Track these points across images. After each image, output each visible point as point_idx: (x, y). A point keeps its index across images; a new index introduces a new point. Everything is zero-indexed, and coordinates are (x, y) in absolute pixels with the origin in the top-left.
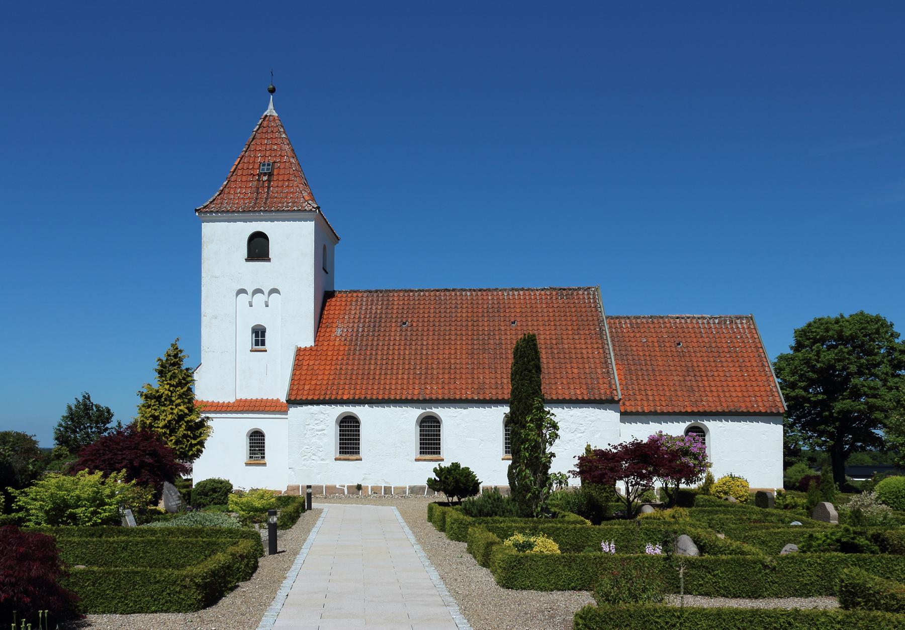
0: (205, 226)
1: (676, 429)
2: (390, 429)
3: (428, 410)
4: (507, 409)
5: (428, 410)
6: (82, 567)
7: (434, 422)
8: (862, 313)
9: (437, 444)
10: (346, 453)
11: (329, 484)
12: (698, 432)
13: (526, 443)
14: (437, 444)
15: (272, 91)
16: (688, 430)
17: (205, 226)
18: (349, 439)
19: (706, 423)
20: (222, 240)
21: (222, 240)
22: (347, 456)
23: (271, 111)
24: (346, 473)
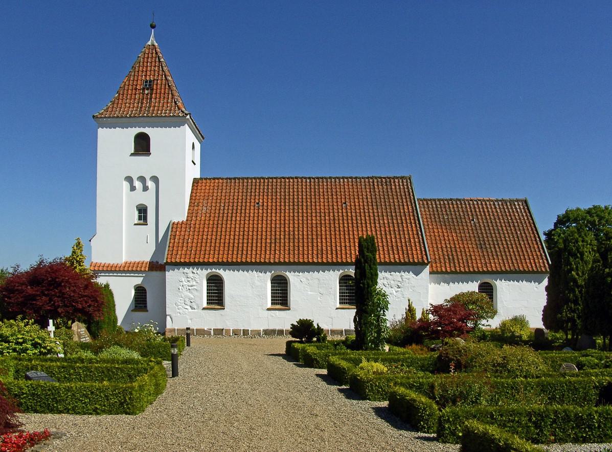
0: (100, 130)
1: (472, 287)
2: (248, 289)
3: (214, 270)
4: (545, 282)
5: (214, 270)
6: (433, 336)
7: (282, 280)
8: (558, 216)
9: (210, 300)
10: (212, 303)
11: (199, 327)
12: (487, 289)
13: (360, 293)
14: (210, 300)
15: (153, 27)
16: (480, 286)
17: (100, 130)
18: (216, 295)
19: (288, 274)
20: (114, 142)
21: (114, 142)
22: (213, 306)
23: (152, 41)
24: (211, 320)
